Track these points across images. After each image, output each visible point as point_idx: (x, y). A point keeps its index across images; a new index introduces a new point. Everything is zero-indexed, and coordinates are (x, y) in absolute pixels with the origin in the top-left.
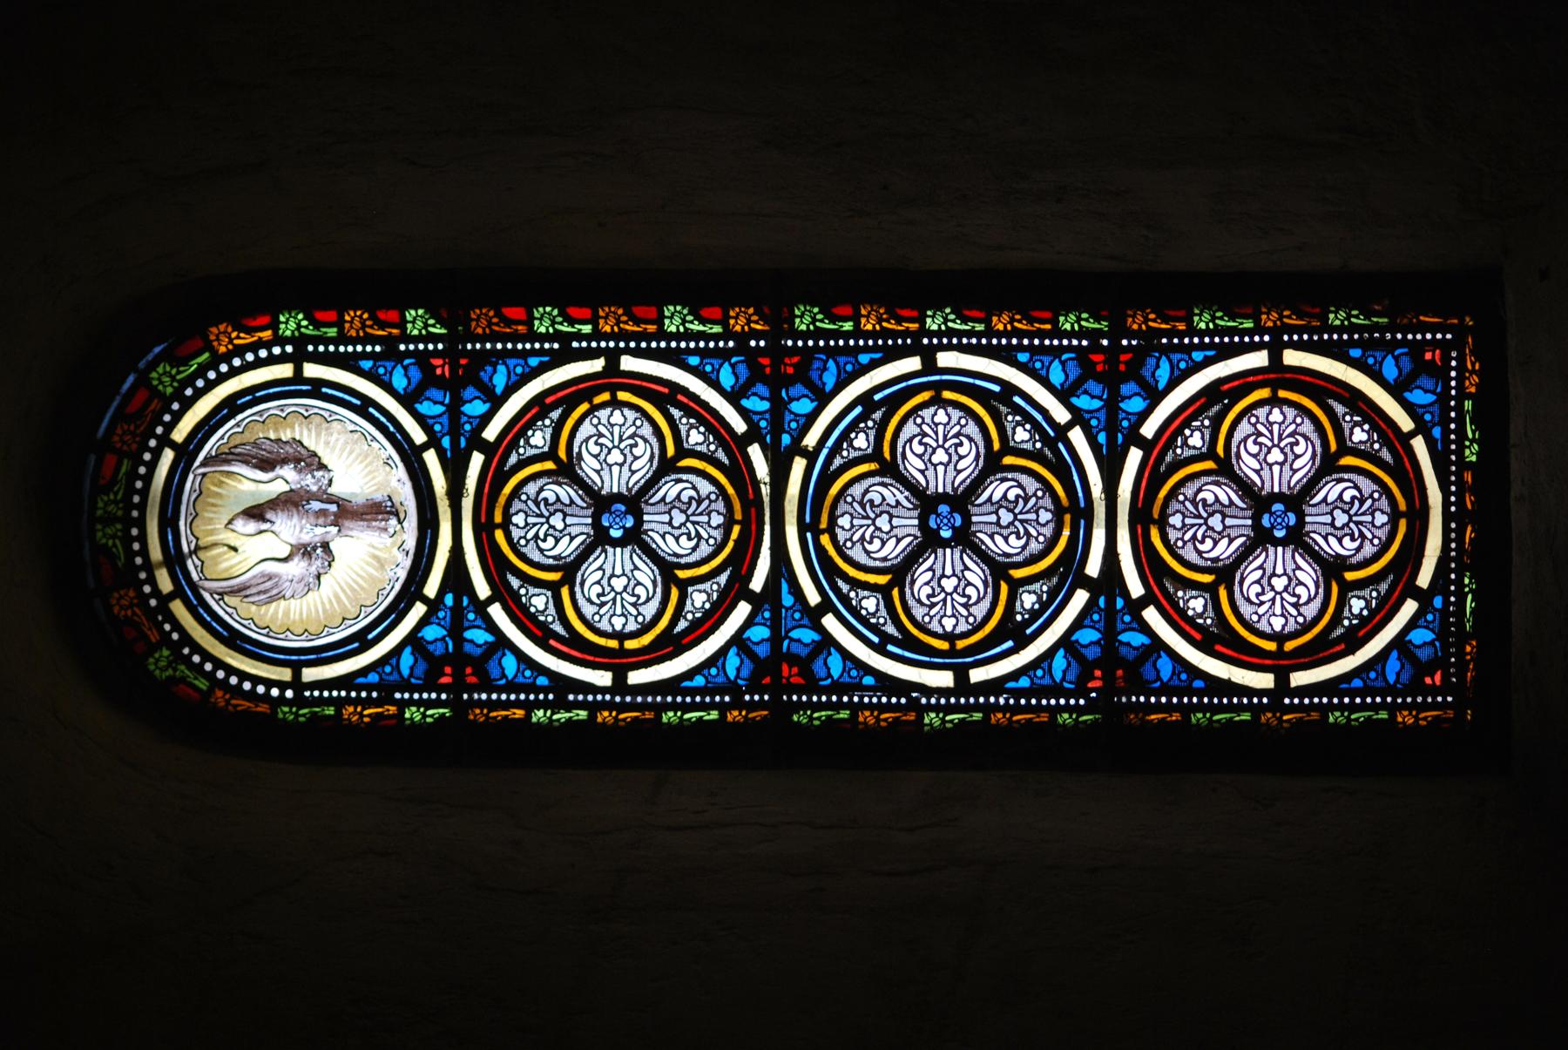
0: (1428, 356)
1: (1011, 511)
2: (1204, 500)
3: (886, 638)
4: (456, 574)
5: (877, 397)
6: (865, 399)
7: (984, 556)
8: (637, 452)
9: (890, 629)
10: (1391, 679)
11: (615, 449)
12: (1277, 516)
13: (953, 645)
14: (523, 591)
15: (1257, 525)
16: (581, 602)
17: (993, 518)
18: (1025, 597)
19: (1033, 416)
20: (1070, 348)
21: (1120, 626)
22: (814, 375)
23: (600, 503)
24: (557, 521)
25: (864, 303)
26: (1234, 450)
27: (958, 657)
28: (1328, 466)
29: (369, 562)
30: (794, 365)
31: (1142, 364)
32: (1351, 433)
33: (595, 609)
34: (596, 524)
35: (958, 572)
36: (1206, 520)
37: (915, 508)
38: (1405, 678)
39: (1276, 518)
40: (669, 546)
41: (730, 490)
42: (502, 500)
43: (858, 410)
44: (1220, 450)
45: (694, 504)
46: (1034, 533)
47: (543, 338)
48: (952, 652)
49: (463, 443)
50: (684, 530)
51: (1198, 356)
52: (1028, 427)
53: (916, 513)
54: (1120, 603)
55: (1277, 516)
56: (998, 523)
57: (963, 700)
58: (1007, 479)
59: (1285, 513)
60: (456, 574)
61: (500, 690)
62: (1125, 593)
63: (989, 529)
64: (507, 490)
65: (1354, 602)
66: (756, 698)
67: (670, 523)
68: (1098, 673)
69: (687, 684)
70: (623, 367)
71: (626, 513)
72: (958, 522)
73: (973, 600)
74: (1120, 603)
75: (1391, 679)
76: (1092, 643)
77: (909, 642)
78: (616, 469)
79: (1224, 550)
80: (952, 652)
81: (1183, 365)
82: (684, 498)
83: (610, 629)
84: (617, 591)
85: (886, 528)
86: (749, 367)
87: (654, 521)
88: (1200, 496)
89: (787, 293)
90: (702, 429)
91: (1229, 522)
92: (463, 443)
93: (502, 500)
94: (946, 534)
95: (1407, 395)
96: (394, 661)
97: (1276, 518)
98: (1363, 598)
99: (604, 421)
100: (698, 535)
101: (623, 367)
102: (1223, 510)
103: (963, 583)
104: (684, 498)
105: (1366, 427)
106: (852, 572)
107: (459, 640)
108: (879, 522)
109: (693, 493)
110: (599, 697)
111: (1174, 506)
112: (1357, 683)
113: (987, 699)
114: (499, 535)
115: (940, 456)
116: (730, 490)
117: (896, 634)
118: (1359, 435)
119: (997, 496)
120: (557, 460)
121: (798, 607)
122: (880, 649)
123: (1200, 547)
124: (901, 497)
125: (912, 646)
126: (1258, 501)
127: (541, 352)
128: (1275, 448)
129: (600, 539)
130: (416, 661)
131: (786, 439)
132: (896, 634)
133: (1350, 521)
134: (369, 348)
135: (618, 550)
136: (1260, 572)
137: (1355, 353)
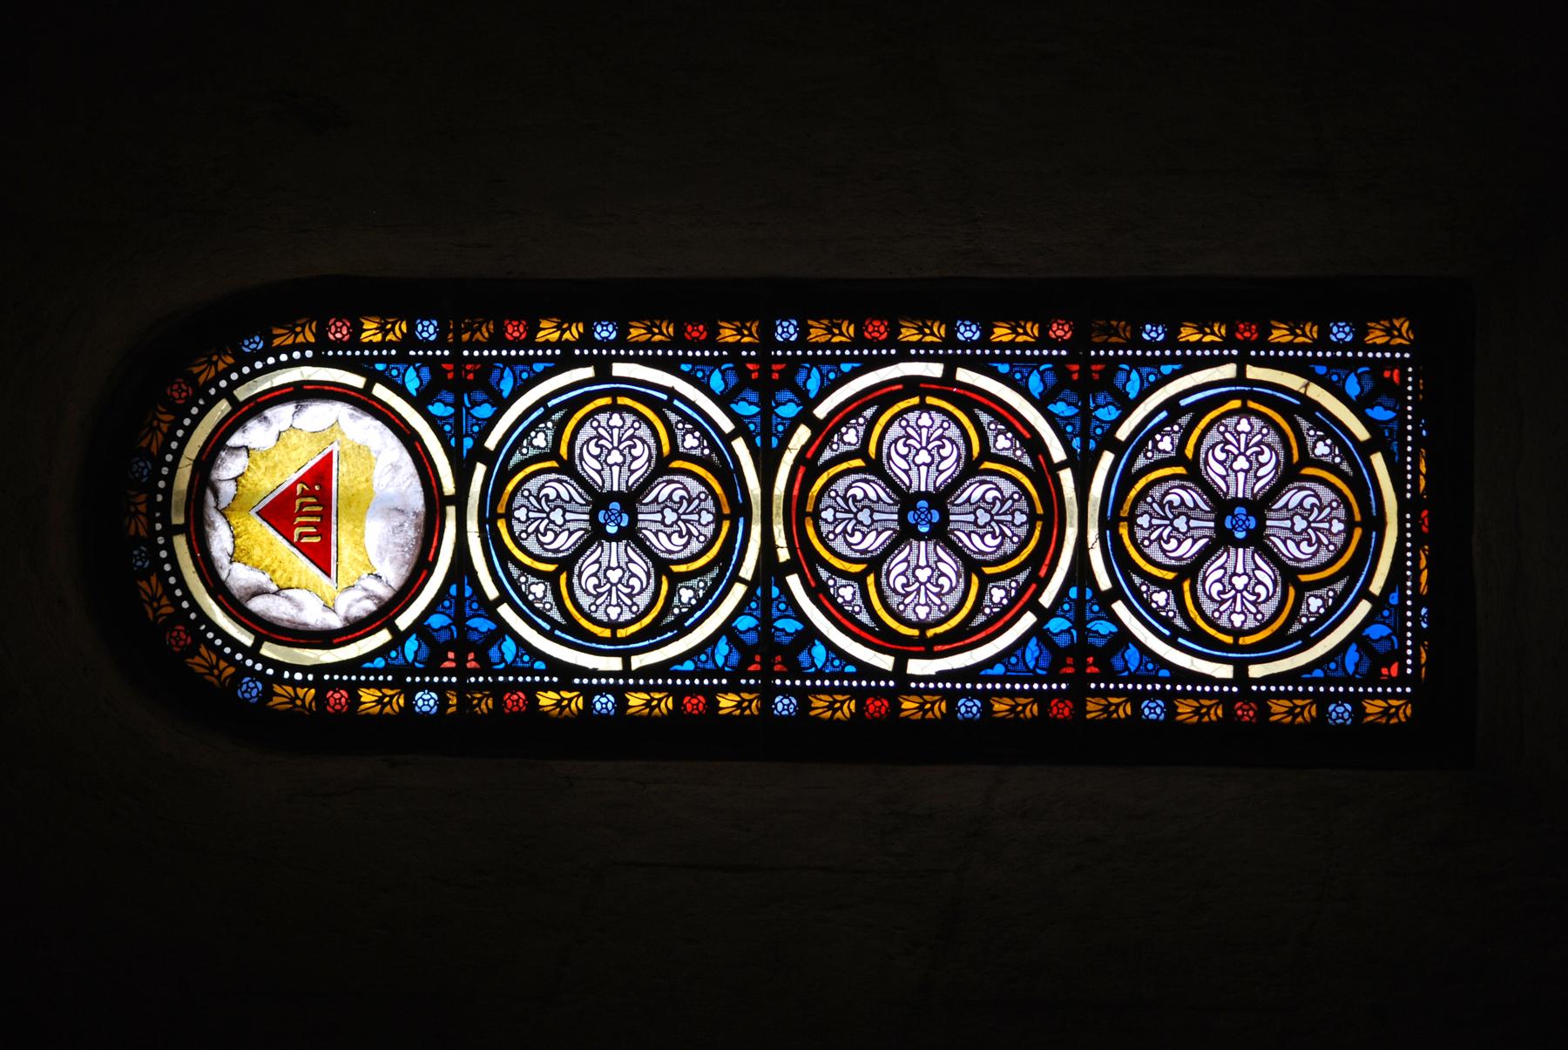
0: (1387, 374)
1: (989, 511)
2: (854, 496)
3: (1177, 632)
4: (1081, 570)
5: (1183, 402)
6: (1171, 404)
7: (957, 551)
8: (635, 452)
9: (1179, 622)
10: (1351, 669)
11: (614, 451)
12: (1236, 525)
13: (614, 633)
14: (831, 582)
15: (902, 519)
16: (578, 593)
17: (1288, 524)
18: (541, 587)
19: (701, 425)
20: (1049, 358)
21: (1089, 615)
22: (493, 381)
23: (598, 499)
24: (557, 516)
25: (369, 314)
26: (885, 451)
27: (1239, 653)
28: (1289, 475)
29: (372, 553)
30: (475, 372)
31: (796, 373)
32: (1314, 447)
33: (592, 600)
34: (593, 519)
35: (931, 563)
36: (1309, 526)
37: (895, 504)
38: (1364, 669)
39: (1239, 522)
40: (662, 544)
41: (718, 489)
42: (505, 497)
43: (1163, 414)
44: (564, 451)
45: (685, 504)
46: (1009, 533)
47: (547, 345)
48: (614, 640)
49: (1092, 445)
50: (675, 528)
51: (846, 367)
52: (697, 434)
53: (895, 509)
54: (1089, 594)
55: (1236, 525)
56: (975, 523)
57: (788, 683)
58: (673, 482)
59: (1234, 516)
60: (1081, 570)
61: (813, 677)
62: (1094, 584)
63: (1283, 534)
64: (510, 487)
65: (683, 591)
66: (1054, 686)
67: (663, 522)
68: (451, 655)
69: (678, 667)
70: (615, 373)
71: (607, 510)
72: (601, 514)
73: (946, 589)
74: (1089, 594)
75: (1351, 669)
76: (749, 630)
77: (1196, 635)
78: (923, 469)
79: (873, 542)
80: (1235, 647)
81: (1152, 378)
82: (676, 497)
83: (605, 619)
84: (925, 583)
85: (560, 521)
86: (1057, 375)
87: (648, 519)
88: (1168, 498)
89: (758, 303)
90: (844, 430)
91: (1193, 523)
92: (1092, 445)
93: (505, 497)
94: (612, 529)
95: (1368, 411)
96: (709, 650)
97: (1239, 522)
98: (1321, 597)
99: (604, 424)
100: (689, 533)
101: (615, 373)
102: (1182, 510)
103: (936, 574)
104: (676, 497)
105: (1158, 437)
106: (527, 561)
107: (458, 405)
108: (552, 516)
109: (683, 493)
110: (603, 681)
111: (1142, 507)
112: (1318, 673)
113: (1346, 690)
114: (501, 525)
115: (615, 457)
116: (718, 489)
117: (1185, 627)
118: (540, 441)
119: (976, 496)
120: (558, 458)
121: (783, 598)
122: (1171, 641)
123: (1166, 547)
124: (883, 495)
125: (571, 631)
126: (1221, 505)
127: (544, 358)
128: (1240, 459)
129: (596, 535)
130: (1361, 658)
131: (468, 443)
132: (1185, 627)
133: (1308, 526)
134: (1207, 353)
135: (614, 544)
136: (596, 566)
137: (1004, 368)
